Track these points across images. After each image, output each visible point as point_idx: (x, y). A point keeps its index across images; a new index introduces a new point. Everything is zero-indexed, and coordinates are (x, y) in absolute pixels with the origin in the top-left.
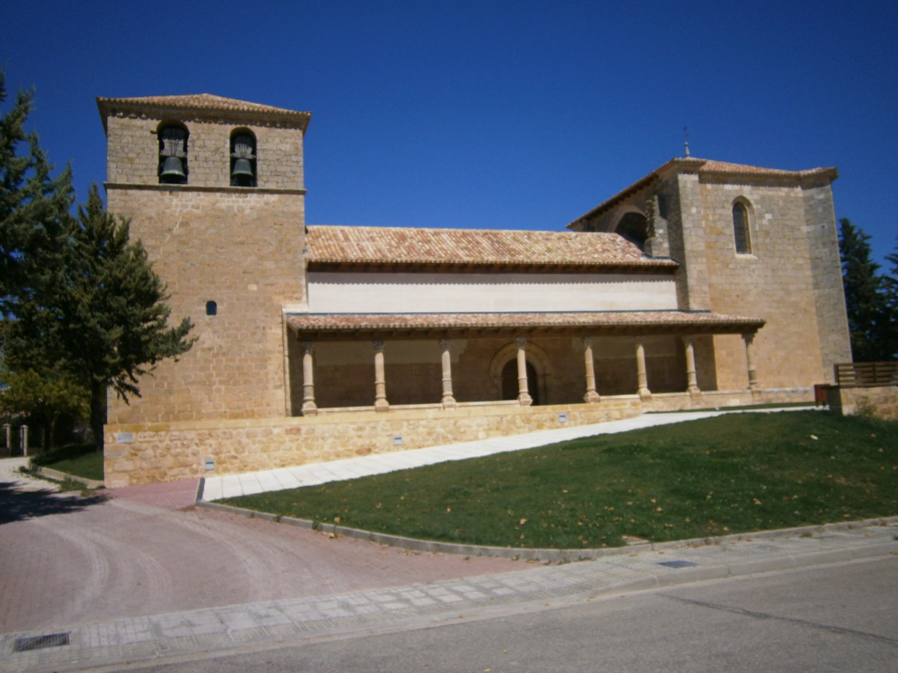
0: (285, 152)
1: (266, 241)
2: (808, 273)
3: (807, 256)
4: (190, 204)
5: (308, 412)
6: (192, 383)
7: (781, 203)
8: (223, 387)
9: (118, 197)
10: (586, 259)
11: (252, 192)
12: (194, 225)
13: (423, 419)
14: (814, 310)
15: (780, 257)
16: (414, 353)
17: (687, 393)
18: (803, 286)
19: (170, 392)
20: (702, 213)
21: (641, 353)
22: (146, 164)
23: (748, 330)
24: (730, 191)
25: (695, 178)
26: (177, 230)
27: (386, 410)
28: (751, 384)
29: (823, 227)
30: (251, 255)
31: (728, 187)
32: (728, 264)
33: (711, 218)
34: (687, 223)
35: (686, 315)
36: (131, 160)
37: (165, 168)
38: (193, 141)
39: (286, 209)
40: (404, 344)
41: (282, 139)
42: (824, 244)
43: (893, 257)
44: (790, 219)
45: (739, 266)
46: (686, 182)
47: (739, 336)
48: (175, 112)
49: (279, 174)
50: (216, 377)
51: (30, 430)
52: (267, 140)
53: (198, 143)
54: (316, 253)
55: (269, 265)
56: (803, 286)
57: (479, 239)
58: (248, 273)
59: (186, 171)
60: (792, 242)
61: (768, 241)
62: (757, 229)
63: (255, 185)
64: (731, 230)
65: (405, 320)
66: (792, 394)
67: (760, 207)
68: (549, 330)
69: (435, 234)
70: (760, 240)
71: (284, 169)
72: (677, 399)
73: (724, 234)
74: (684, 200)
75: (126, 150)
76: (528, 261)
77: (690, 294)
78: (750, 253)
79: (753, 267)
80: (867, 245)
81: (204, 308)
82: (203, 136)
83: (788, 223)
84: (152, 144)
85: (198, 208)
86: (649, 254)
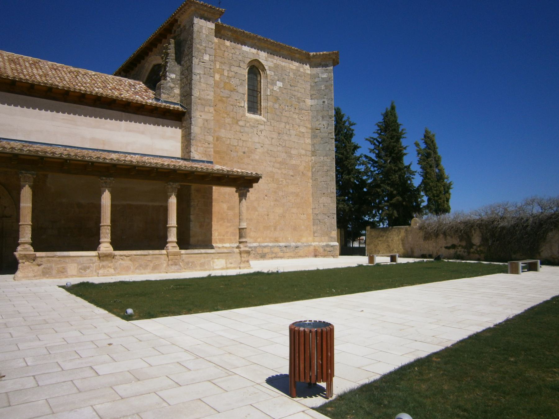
2: (309, 141)
7: (291, 74)
14: (310, 174)
15: (286, 123)
17: (164, 252)
18: (303, 152)
21: (106, 199)
24: (247, 52)
25: (212, 26)
28: (240, 243)
29: (324, 102)
31: (245, 48)
33: (226, 73)
34: (197, 69)
42: (323, 117)
43: (372, 140)
44: (298, 91)
45: (248, 125)
46: (201, 27)
47: (234, 189)
56: (303, 152)
61: (277, 106)
62: (269, 94)
64: (245, 89)
66: (285, 249)
67: (273, 73)
70: (270, 104)
72: (149, 258)
73: (237, 92)
74: (197, 45)
78: (261, 115)
79: (262, 127)
80: (353, 130)
83: (296, 93)
86: (158, 97)
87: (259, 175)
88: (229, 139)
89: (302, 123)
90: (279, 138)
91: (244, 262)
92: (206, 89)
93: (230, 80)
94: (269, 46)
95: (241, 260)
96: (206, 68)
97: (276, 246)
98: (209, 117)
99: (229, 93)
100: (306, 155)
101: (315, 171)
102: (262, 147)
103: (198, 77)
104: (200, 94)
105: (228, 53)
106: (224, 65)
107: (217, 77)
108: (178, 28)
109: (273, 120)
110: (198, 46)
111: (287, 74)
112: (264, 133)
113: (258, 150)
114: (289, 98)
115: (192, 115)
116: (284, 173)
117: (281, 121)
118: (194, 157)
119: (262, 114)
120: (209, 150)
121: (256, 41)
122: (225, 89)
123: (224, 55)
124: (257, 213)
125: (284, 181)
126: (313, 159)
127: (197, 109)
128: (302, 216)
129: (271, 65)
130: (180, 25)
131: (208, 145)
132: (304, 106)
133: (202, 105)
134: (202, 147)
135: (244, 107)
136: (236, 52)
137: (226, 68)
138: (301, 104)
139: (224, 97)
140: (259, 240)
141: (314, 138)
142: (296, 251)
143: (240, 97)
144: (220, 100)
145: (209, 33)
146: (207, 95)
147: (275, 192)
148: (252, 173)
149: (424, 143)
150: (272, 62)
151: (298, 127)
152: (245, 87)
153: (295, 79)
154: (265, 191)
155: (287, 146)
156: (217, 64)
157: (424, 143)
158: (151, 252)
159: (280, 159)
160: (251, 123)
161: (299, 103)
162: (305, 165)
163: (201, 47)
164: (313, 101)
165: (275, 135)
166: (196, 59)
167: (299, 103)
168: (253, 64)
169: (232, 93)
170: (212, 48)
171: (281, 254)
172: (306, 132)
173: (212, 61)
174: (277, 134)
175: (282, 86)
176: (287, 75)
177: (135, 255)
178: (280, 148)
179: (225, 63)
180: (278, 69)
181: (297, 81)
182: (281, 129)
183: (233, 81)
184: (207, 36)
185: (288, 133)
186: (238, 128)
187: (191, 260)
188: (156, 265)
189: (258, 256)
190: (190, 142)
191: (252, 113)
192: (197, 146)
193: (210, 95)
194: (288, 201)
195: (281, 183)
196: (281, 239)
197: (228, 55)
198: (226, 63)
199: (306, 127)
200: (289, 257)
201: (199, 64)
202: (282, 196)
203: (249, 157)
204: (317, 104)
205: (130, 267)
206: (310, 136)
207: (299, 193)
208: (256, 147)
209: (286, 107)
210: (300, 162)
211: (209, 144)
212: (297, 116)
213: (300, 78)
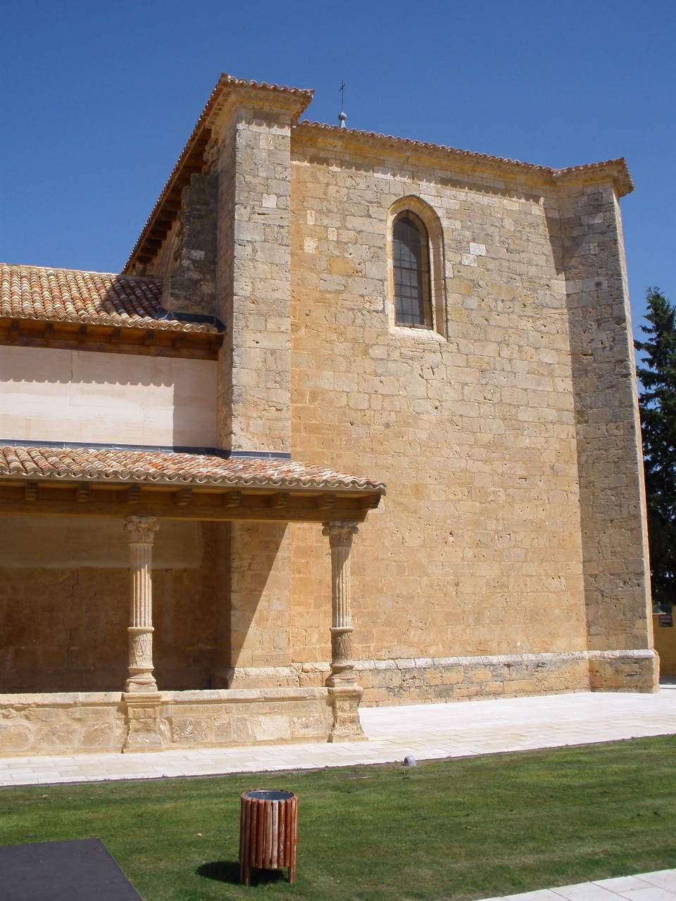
2: (568, 385)
3: (566, 347)
7: (508, 224)
14: (573, 471)
15: (499, 343)
17: (116, 696)
18: (552, 414)
29: (598, 284)
32: (368, 346)
33: (332, 236)
42: (599, 323)
44: (530, 263)
45: (396, 355)
56: (552, 414)
60: (529, 311)
61: (473, 302)
72: (78, 712)
74: (244, 177)
77: (237, 408)
79: (436, 358)
83: (522, 268)
87: (375, 486)
88: (345, 394)
89: (545, 341)
90: (483, 382)
91: (343, 722)
92: (269, 277)
93: (344, 250)
94: (445, 162)
95: (335, 718)
96: (269, 226)
97: (479, 664)
98: (282, 343)
99: (343, 282)
102: (436, 408)
103: (249, 249)
104: (253, 290)
105: (336, 188)
106: (327, 217)
109: (465, 337)
110: (249, 178)
111: (497, 224)
112: (441, 373)
113: (424, 417)
115: (234, 342)
116: (500, 471)
117: (486, 340)
118: (240, 446)
119: (435, 326)
121: (408, 154)
122: (330, 273)
123: (326, 194)
125: (502, 493)
126: (581, 432)
127: (247, 326)
128: (556, 582)
129: (454, 204)
131: (277, 413)
132: (548, 298)
135: (383, 311)
136: (358, 184)
138: (541, 292)
139: (330, 292)
140: (432, 650)
141: (581, 376)
142: (539, 675)
144: (316, 301)
145: (275, 147)
146: (274, 290)
147: (476, 523)
148: (354, 482)
149: (641, 394)
150: (455, 198)
151: (533, 350)
152: (385, 261)
153: (518, 234)
154: (449, 522)
156: (308, 216)
157: (641, 394)
158: (81, 696)
159: (487, 437)
160: (403, 350)
161: (535, 291)
162: (557, 446)
163: (255, 181)
164: (571, 282)
165: (471, 377)
166: (242, 210)
167: (535, 291)
169: (350, 280)
170: (283, 179)
171: (495, 685)
172: (558, 363)
173: (285, 209)
176: (496, 227)
177: (38, 706)
178: (486, 409)
179: (329, 211)
180: (471, 214)
181: (524, 238)
182: (486, 359)
183: (351, 250)
184: (270, 153)
185: (508, 367)
186: (368, 365)
187: (190, 717)
188: (96, 730)
189: (431, 691)
190: (231, 409)
191: (407, 324)
193: (282, 289)
194: (513, 543)
195: (491, 498)
196: (495, 645)
197: (338, 192)
198: (332, 212)
199: (557, 350)
200: (517, 693)
201: (250, 219)
202: (497, 532)
204: (582, 291)
205: (26, 736)
206: (570, 372)
207: (545, 522)
208: (418, 410)
209: (500, 303)
210: (543, 440)
211: (277, 410)
212: (529, 325)
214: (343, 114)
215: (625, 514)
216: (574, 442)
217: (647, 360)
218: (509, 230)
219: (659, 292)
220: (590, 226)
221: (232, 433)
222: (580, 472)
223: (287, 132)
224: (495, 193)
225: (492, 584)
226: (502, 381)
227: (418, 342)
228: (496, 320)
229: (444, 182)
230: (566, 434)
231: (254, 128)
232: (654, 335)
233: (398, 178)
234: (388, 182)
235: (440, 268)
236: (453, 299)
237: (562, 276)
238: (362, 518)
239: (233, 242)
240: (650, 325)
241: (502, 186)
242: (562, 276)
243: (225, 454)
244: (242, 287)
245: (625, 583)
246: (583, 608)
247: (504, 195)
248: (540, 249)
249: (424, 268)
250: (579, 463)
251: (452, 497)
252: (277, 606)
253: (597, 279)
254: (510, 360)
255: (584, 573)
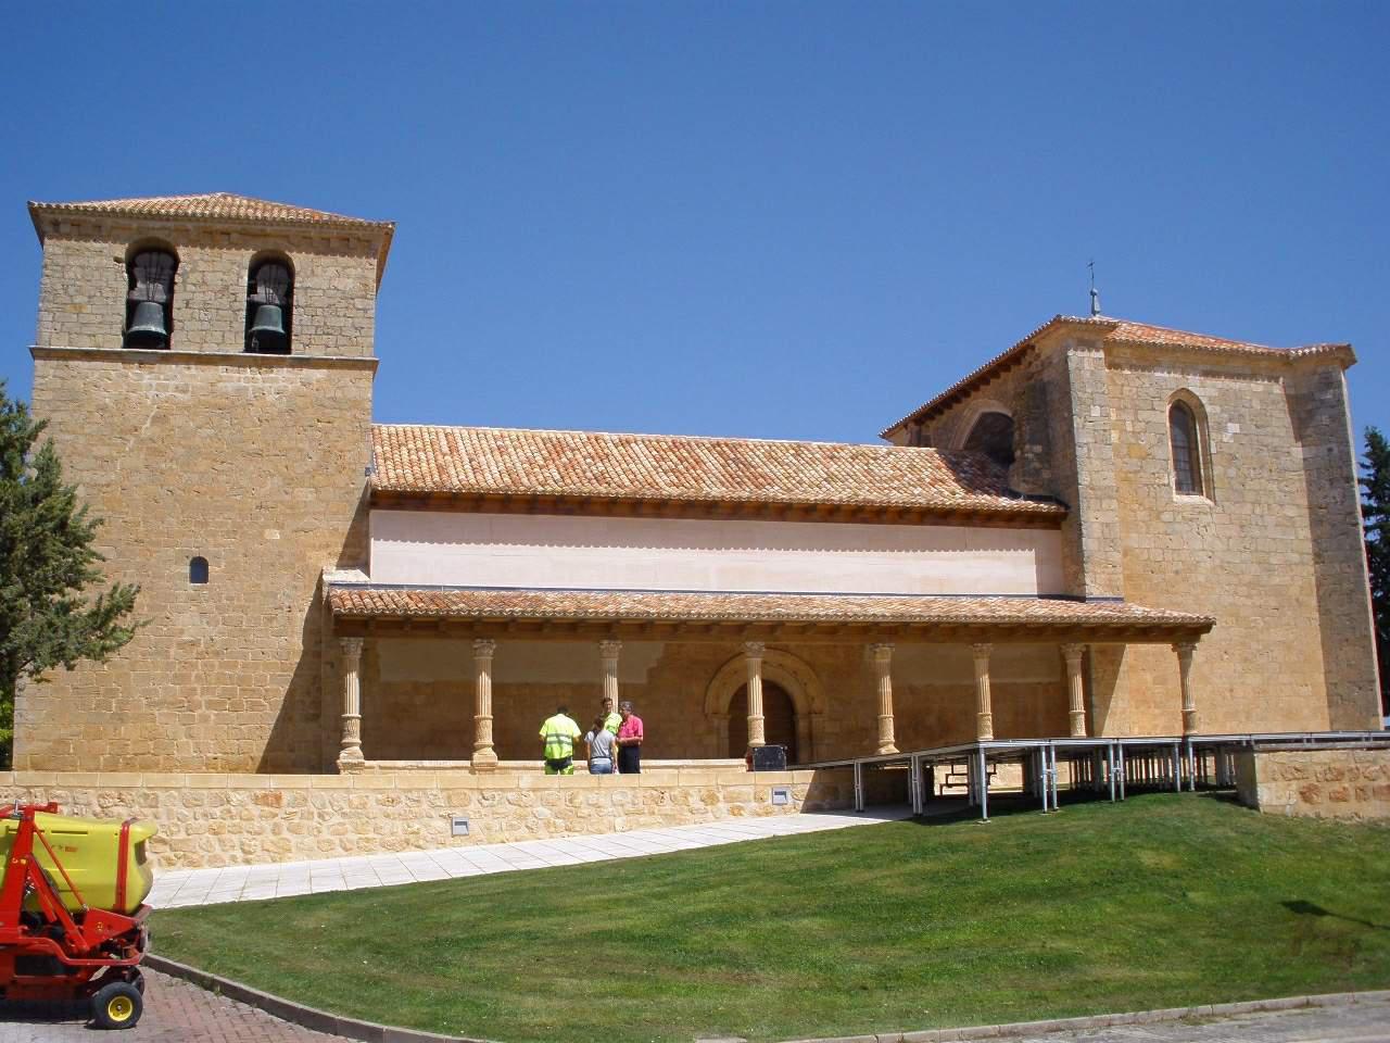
0: (344, 292)
1: (300, 450)
2: (1305, 533)
3: (1304, 502)
4: (172, 383)
5: (351, 767)
6: (156, 704)
7: (1257, 405)
8: (212, 714)
9: (52, 371)
10: (897, 497)
11: (280, 363)
12: (177, 421)
13: (511, 790)
14: (1314, 602)
15: (1253, 503)
16: (404, 661)
18: (1295, 557)
19: (121, 718)
20: (1113, 417)
22: (103, 315)
23: (1184, 635)
26: (147, 430)
27: (491, 768)
29: (1330, 450)
30: (272, 476)
35: (1074, 605)
36: (78, 309)
37: (257, 321)
38: (185, 273)
39: (339, 394)
40: (525, 646)
41: (339, 269)
42: (1331, 481)
44: (1273, 436)
48: (158, 224)
49: (330, 331)
50: (202, 694)
51: (933, 791)
52: (313, 271)
53: (193, 278)
54: (392, 474)
55: (305, 494)
56: (1295, 557)
57: (703, 454)
58: (267, 508)
59: (168, 323)
61: (1232, 472)
63: (288, 351)
65: (540, 601)
68: (677, 628)
69: (625, 443)
71: (341, 322)
75: (71, 290)
76: (784, 496)
79: (1205, 519)
81: (187, 570)
82: (202, 266)
83: (1269, 440)
84: (116, 280)
85: (184, 392)
90: (1243, 535)
100: (1303, 563)
101: (1324, 594)
103: (1085, 449)
105: (1128, 388)
107: (1114, 436)
108: (1036, 360)
110: (1080, 394)
112: (1212, 530)
113: (1202, 564)
114: (1255, 451)
116: (1258, 603)
120: (1116, 577)
123: (1122, 394)
124: (1209, 687)
130: (1038, 356)
133: (1097, 498)
134: (1104, 572)
135: (1168, 485)
137: (1128, 417)
143: (1159, 466)
147: (1243, 644)
150: (1214, 387)
155: (1260, 548)
159: (1247, 578)
165: (1233, 531)
168: (1177, 398)
170: (1103, 393)
174: (1239, 529)
175: (1238, 431)
178: (1246, 556)
184: (1092, 372)
186: (1162, 528)
192: (1095, 573)
193: (1109, 479)
195: (1253, 625)
199: (1298, 505)
201: (1084, 426)
202: (1259, 651)
203: (1185, 580)
213: (1274, 407)
214: (1095, 291)
215: (1358, 635)
216: (1313, 579)
217: (1366, 494)
218: (1256, 410)
219: (1377, 431)
220: (1322, 402)
221: (1085, 584)
222: (1319, 602)
223: (1101, 354)
224: (1244, 379)
225: (1258, 690)
226: (1257, 533)
227: (1194, 507)
228: (1250, 484)
229: (1206, 374)
230: (1308, 572)
231: (1079, 354)
232: (1372, 471)
233: (1172, 375)
234: (1165, 379)
235: (1206, 447)
236: (1217, 471)
237: (1300, 444)
238: (1197, 639)
239: (1075, 445)
240: (1368, 462)
241: (1248, 371)
242: (1300, 444)
243: (1082, 599)
244: (1084, 479)
245: (1360, 688)
246: (1326, 711)
247: (1251, 379)
248: (1281, 421)
249: (1193, 446)
250: (1318, 596)
251: (1224, 624)
252: (1120, 704)
253: (1329, 446)
254: (1262, 516)
255: (1326, 683)
